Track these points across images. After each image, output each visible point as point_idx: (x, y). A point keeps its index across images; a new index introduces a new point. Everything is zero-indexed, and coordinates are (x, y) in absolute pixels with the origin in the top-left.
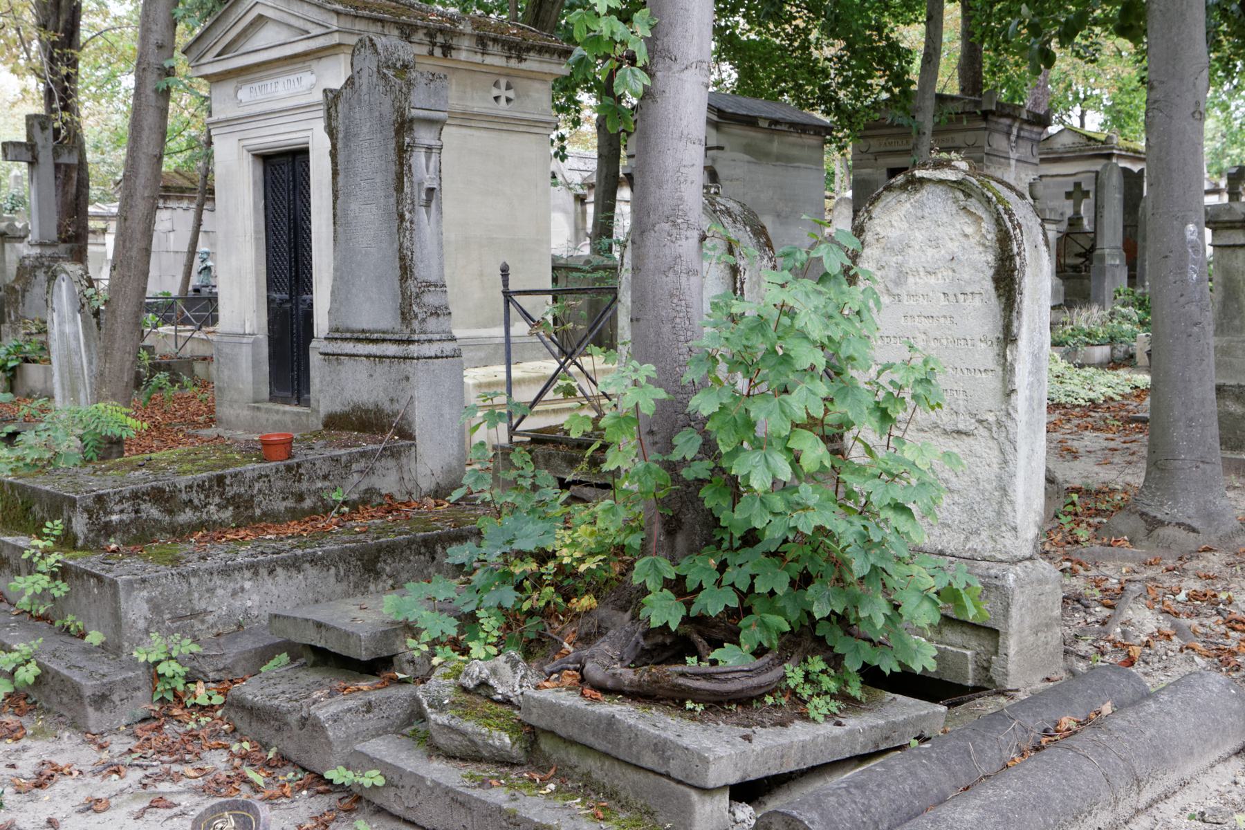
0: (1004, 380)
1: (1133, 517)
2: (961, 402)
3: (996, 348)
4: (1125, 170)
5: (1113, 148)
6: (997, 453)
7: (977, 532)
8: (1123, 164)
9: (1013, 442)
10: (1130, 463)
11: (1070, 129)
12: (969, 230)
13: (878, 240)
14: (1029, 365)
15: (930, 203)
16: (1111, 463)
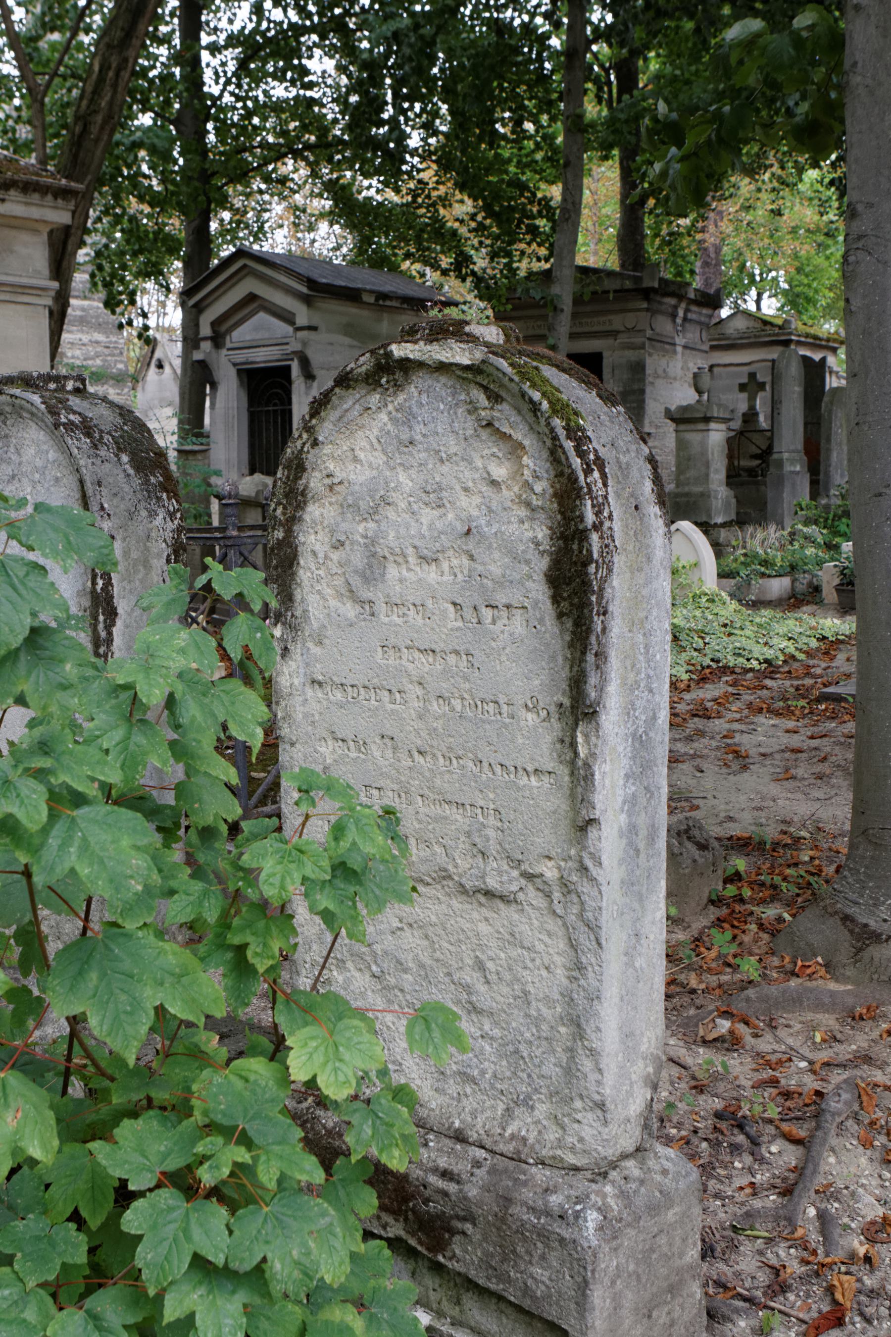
0: (572, 796)
1: (831, 921)
2: (491, 833)
3: (557, 725)
4: (805, 359)
5: (791, 334)
6: (562, 945)
7: (526, 1103)
8: (803, 352)
9: (593, 928)
10: (820, 777)
11: (747, 314)
12: (500, 472)
13: (331, 488)
14: (625, 762)
15: (424, 414)
16: (794, 778)
